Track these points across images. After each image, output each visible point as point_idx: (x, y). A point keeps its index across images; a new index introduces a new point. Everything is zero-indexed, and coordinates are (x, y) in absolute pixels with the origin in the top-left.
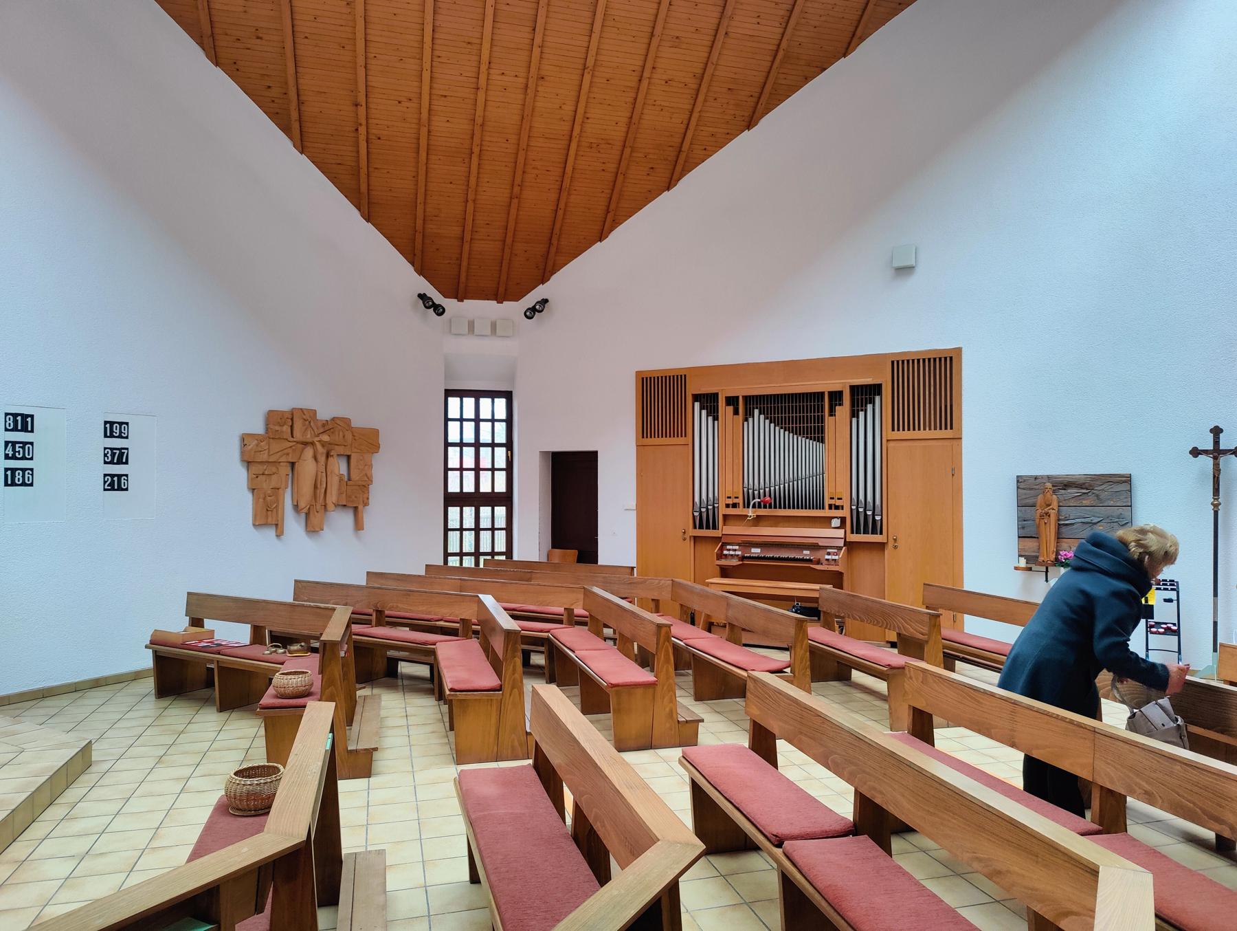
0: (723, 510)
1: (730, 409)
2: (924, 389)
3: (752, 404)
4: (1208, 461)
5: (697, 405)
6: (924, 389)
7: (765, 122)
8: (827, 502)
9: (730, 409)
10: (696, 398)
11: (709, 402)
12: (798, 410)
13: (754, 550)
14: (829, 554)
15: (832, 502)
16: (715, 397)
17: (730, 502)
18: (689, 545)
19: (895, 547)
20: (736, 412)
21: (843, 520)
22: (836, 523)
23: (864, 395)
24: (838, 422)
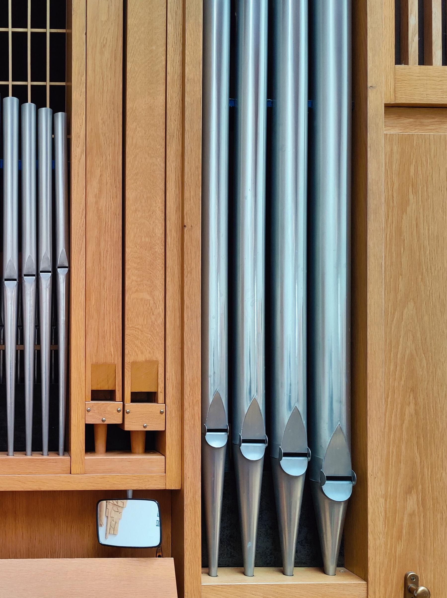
8: (84, 412)
15: (107, 413)
21: (170, 503)
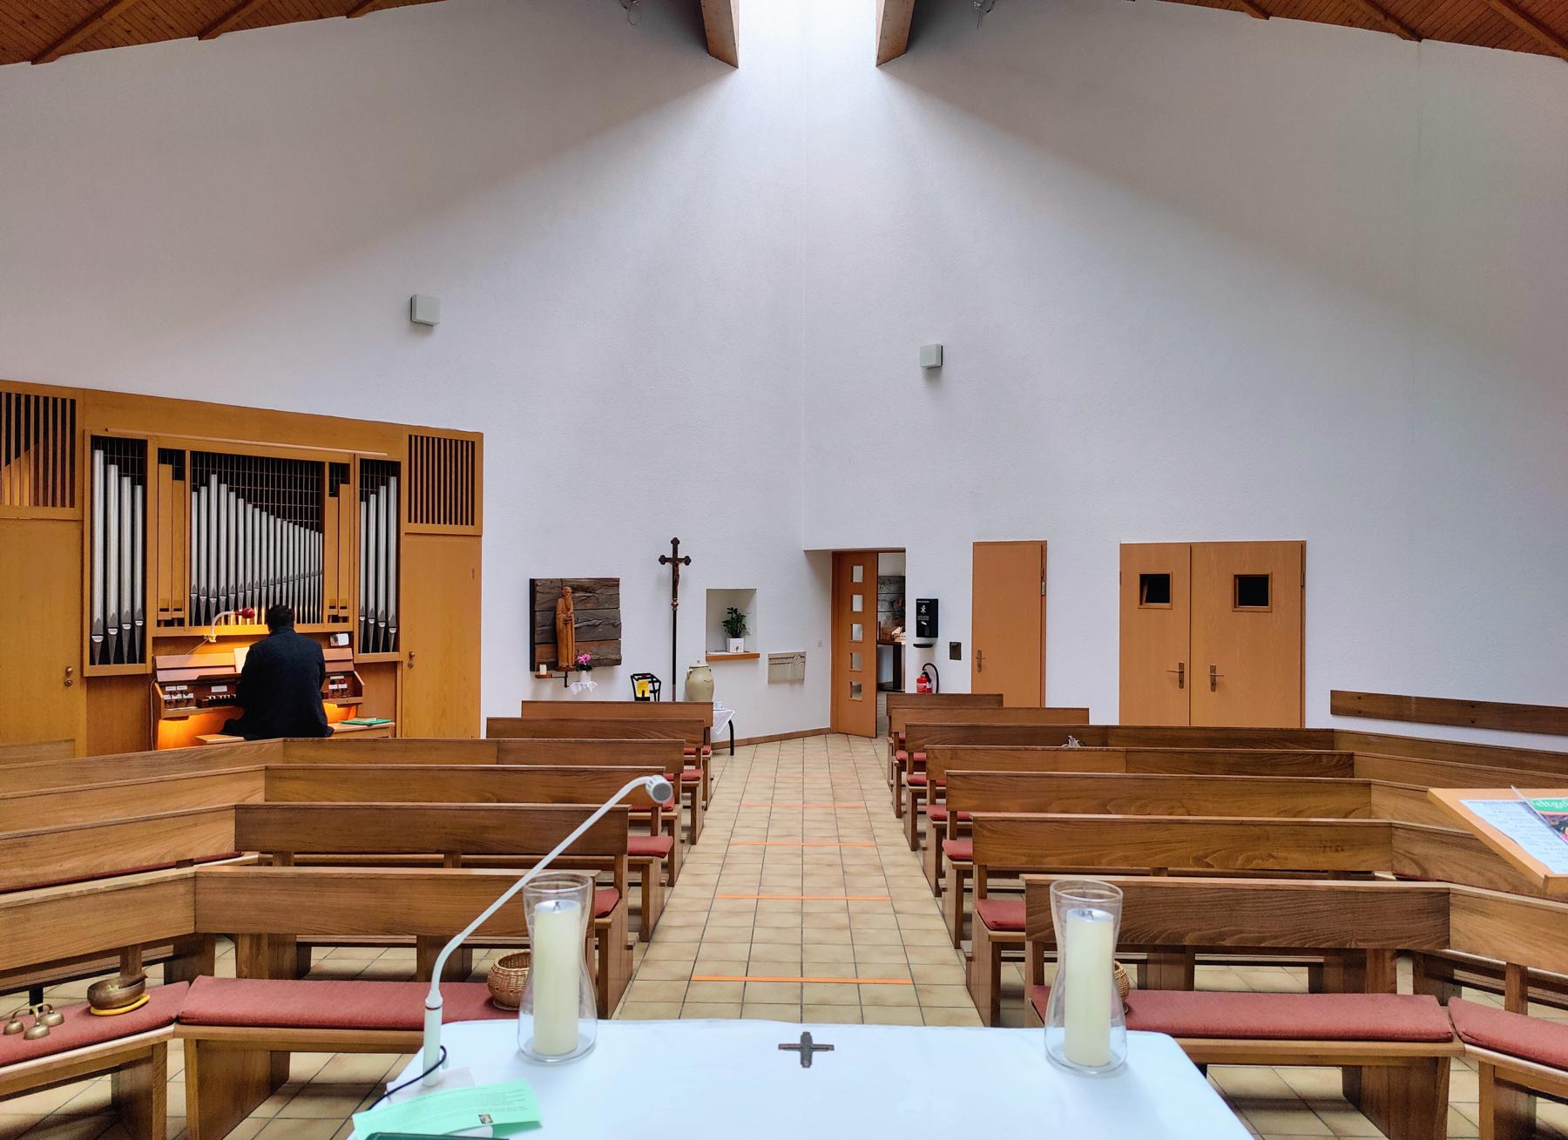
0: (153, 631)
1: (167, 470)
2: (442, 476)
3: (199, 468)
4: (668, 566)
5: (99, 456)
6: (442, 476)
7: (230, 42)
8: (327, 612)
9: (167, 470)
10: (97, 442)
11: (128, 456)
12: (289, 484)
13: (214, 689)
14: (333, 682)
15: (334, 612)
16: (141, 445)
17: (166, 616)
18: (80, 695)
19: (410, 666)
20: (178, 475)
21: (351, 634)
22: (343, 639)
23: (377, 473)
24: (341, 506)
